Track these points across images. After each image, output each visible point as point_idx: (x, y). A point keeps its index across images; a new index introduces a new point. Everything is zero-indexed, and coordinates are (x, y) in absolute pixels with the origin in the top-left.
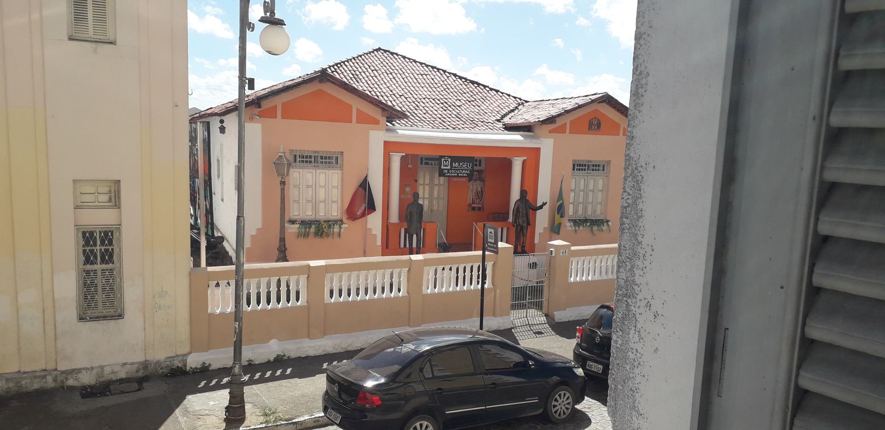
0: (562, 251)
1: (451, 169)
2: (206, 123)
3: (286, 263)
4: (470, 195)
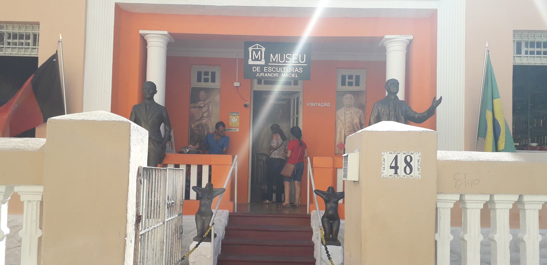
0: (389, 158)
1: (266, 64)
2: (498, 150)
3: (22, 250)
4: (341, 130)
